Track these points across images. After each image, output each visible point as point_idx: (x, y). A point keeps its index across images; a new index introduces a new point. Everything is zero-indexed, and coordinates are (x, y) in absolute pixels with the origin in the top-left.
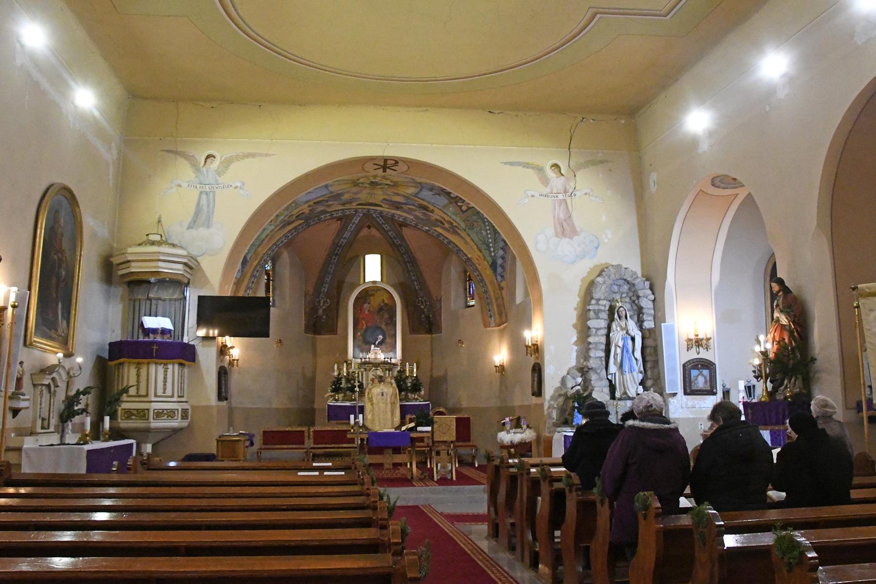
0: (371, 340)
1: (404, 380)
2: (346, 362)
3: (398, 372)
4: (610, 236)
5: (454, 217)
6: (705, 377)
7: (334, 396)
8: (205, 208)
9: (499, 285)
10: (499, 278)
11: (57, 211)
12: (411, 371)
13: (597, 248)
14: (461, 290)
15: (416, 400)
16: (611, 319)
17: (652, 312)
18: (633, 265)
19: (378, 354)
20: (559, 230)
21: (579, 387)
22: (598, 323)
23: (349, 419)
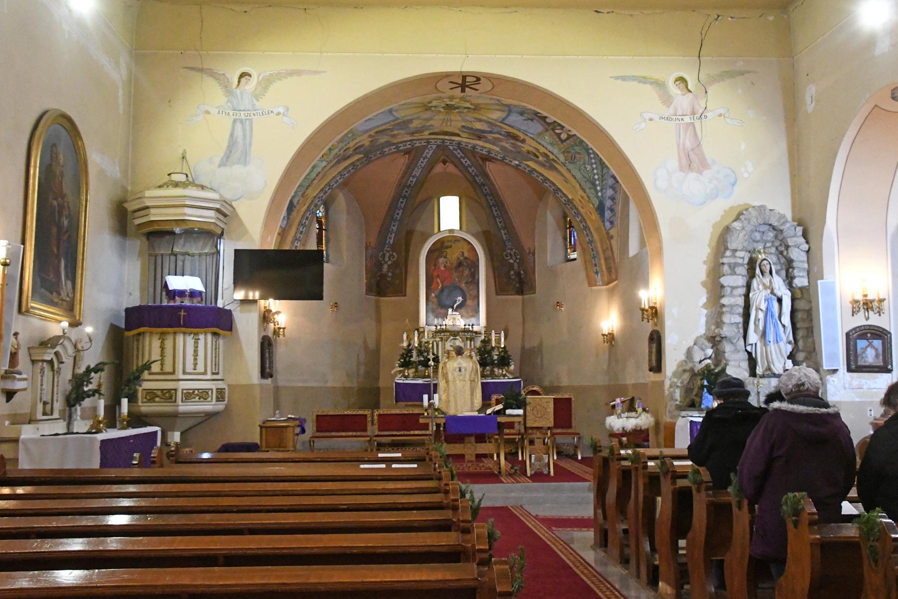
0: (447, 303)
1: (489, 353)
2: (418, 330)
3: (482, 341)
4: (750, 169)
5: (550, 148)
6: (876, 350)
7: (403, 372)
8: (240, 140)
9: (608, 233)
10: (607, 224)
11: (54, 145)
12: (498, 341)
13: (733, 185)
14: (560, 241)
15: (504, 376)
16: (751, 275)
17: (806, 266)
18: (782, 206)
19: (456, 320)
20: (684, 162)
21: (709, 361)
22: (735, 281)
23: (422, 400)
